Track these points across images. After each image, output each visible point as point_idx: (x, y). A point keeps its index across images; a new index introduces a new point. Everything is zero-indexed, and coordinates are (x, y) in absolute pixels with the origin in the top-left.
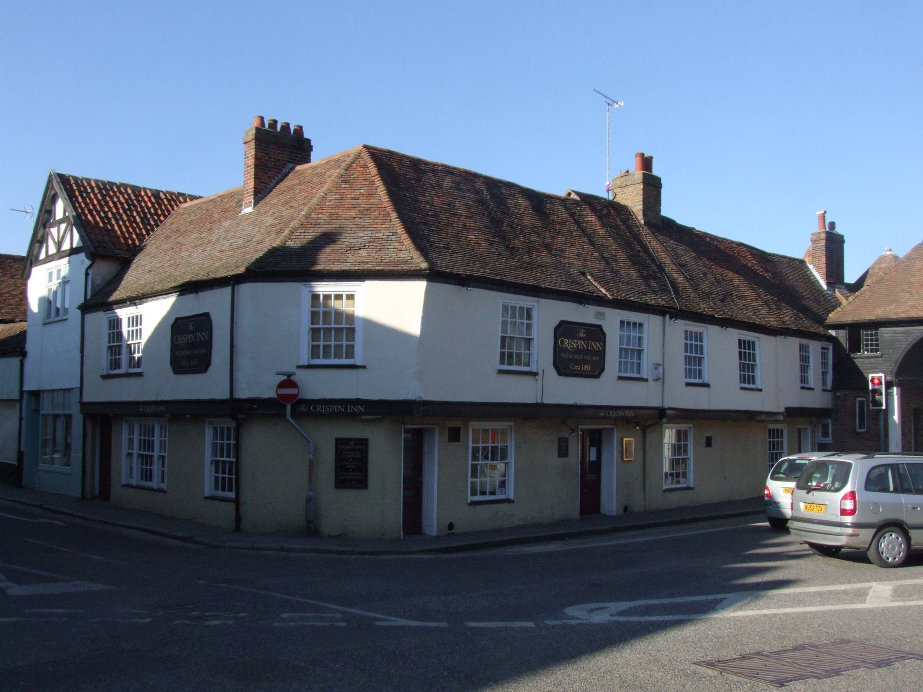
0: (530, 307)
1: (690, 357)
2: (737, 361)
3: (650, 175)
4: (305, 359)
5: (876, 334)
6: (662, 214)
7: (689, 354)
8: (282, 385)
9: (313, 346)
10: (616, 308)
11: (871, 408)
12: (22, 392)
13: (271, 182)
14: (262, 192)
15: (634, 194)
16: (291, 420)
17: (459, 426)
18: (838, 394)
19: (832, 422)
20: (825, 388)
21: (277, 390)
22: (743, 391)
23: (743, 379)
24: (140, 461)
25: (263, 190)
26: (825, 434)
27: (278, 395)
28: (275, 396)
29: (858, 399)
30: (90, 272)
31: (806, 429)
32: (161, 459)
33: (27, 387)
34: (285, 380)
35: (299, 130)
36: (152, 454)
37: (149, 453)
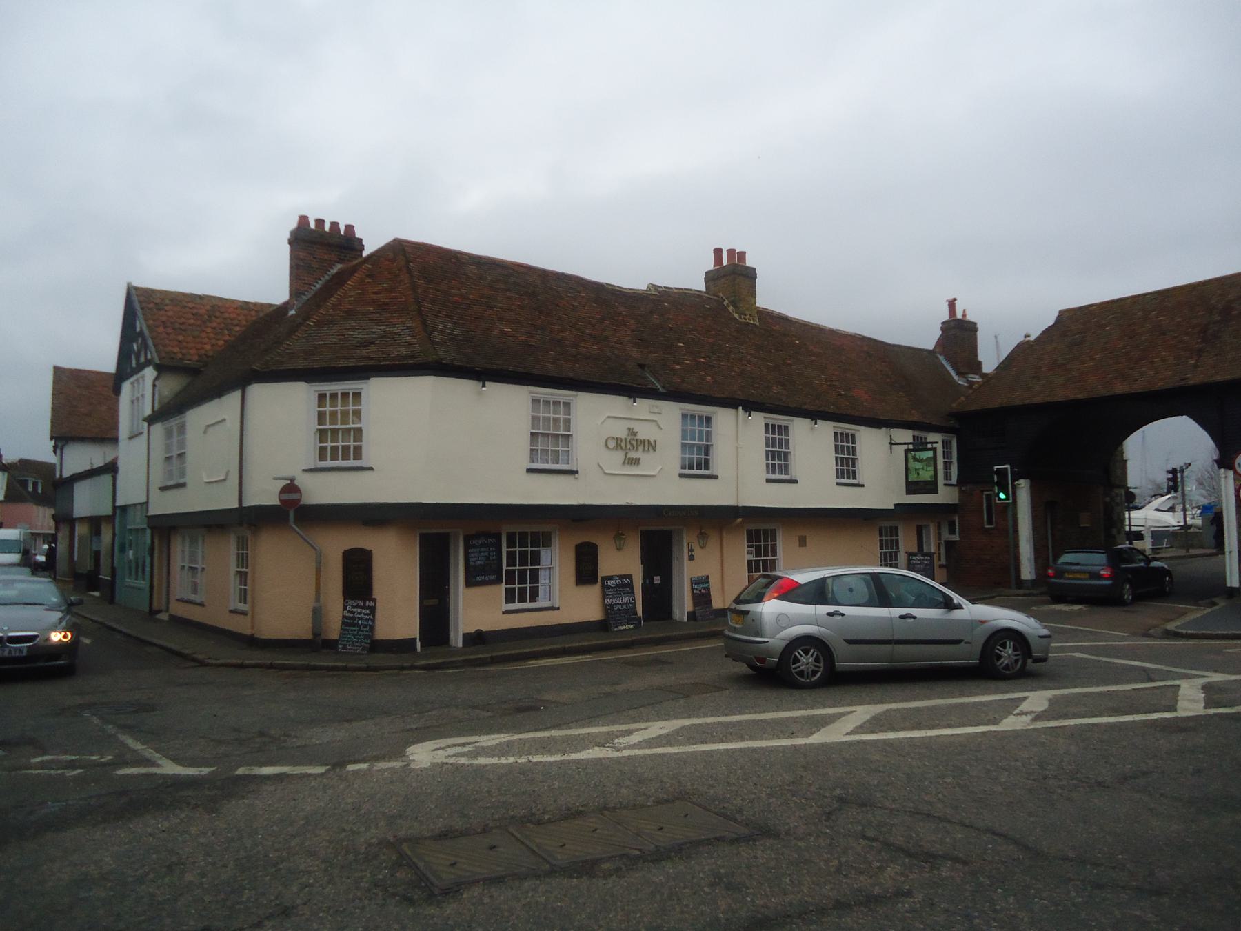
0: (357, 391)
1: (773, 452)
2: (833, 455)
3: (743, 266)
4: (313, 462)
5: (357, 395)
6: (758, 305)
7: (771, 449)
8: (285, 490)
9: (321, 448)
10: (54, 377)
11: (998, 502)
12: (114, 508)
13: (317, 283)
14: (306, 293)
15: (725, 285)
16: (294, 526)
17: (549, 530)
18: (963, 488)
19: (959, 518)
20: (949, 482)
21: (279, 496)
22: (769, 484)
23: (772, 468)
24: (238, 579)
25: (308, 292)
26: (952, 532)
27: (281, 501)
28: (277, 502)
29: (985, 493)
30: (157, 383)
31: (927, 526)
32: (238, 576)
33: (118, 504)
34: (289, 484)
35: (350, 228)
36: (247, 570)
37: (242, 570)
